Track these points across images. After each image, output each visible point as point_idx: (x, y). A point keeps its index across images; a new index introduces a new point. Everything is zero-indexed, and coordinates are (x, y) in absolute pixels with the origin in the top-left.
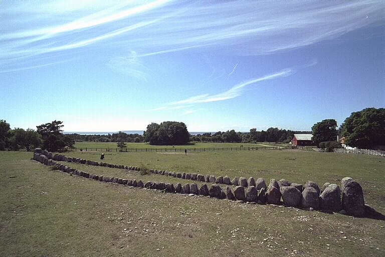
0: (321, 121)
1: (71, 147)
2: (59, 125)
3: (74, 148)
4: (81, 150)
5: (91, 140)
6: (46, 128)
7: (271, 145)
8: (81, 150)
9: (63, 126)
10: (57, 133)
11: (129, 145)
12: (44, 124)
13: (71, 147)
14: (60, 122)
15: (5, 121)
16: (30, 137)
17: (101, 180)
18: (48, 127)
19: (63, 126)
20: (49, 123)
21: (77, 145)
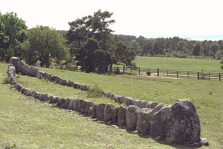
0: (62, 30)
1: (129, 63)
2: (107, 20)
3: (135, 68)
4: (149, 74)
5: (206, 54)
6: (84, 25)
7: (142, 73)
8: (149, 74)
9: (113, 21)
10: (106, 35)
11: (140, 61)
12: (81, 18)
13: (129, 63)
14: (107, 15)
15: (7, 13)
16: (47, 41)
17: (36, 96)
18: (88, 24)
19: (113, 21)
20: (90, 17)
21: (140, 61)
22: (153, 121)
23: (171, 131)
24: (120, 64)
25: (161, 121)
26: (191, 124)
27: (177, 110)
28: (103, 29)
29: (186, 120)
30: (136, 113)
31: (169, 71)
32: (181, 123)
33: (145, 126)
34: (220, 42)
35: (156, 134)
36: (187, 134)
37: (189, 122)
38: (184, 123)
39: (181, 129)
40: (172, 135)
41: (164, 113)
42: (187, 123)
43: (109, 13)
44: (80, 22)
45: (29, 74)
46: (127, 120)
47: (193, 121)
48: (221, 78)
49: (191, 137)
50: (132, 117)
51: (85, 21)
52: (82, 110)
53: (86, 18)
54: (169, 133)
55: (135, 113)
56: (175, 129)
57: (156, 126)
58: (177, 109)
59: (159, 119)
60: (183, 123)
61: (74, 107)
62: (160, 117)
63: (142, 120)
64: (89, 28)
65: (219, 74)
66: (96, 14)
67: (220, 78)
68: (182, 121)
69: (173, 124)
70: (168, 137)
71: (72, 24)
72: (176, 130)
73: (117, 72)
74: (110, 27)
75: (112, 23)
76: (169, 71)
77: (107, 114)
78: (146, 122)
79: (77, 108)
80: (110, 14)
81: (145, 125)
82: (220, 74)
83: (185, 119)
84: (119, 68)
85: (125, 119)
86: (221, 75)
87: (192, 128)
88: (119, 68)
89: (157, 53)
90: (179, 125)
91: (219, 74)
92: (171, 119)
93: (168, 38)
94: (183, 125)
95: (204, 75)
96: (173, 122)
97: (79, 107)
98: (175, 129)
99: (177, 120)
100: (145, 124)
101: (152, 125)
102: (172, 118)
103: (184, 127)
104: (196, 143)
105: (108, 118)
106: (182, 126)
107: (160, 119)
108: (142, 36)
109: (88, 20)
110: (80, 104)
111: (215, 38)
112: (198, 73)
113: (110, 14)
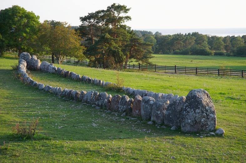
2: (122, 14)
26: (206, 113)
27: (193, 100)
30: (151, 104)
31: (187, 68)
32: (196, 113)
34: (243, 37)
36: (202, 124)
37: (205, 112)
38: (200, 112)
39: (196, 119)
42: (203, 112)
45: (41, 69)
47: (209, 111)
48: (243, 75)
49: (207, 126)
52: (96, 103)
56: (190, 119)
58: (193, 99)
59: (174, 109)
60: (198, 113)
61: (88, 100)
63: (157, 110)
65: (241, 71)
67: (242, 75)
68: (197, 111)
69: (188, 113)
70: (183, 127)
71: (83, 19)
74: (126, 23)
75: (128, 19)
76: (187, 68)
78: (161, 113)
79: (91, 101)
80: (127, 8)
82: (242, 71)
85: (140, 110)
86: (243, 71)
87: (207, 117)
90: (194, 114)
91: (241, 71)
92: (186, 108)
93: (187, 34)
94: (198, 115)
95: (224, 70)
99: (192, 110)
102: (187, 108)
103: (199, 116)
104: (212, 133)
106: (197, 115)
107: (175, 109)
108: (159, 32)
109: (102, 14)
111: (239, 34)
112: (219, 69)
113: (127, 8)
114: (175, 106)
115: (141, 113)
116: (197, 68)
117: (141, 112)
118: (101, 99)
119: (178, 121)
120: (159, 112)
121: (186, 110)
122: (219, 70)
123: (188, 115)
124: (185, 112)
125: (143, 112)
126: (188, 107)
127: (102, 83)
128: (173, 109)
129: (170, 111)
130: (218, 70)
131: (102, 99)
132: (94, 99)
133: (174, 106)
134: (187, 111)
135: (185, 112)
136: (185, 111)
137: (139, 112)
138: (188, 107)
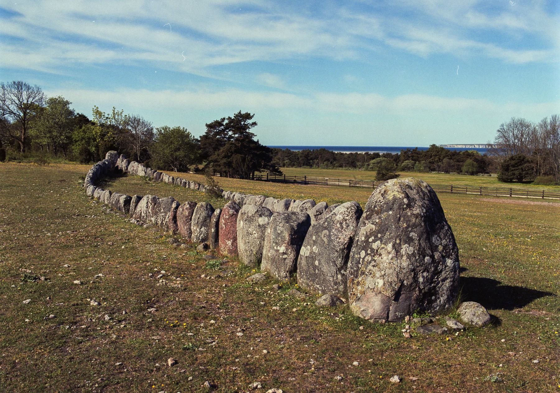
2: (250, 121)
12: (219, 119)
14: (248, 116)
18: (228, 127)
20: (229, 118)
22: (309, 247)
23: (369, 282)
24: (263, 171)
25: (334, 245)
27: (391, 213)
28: (244, 133)
29: (420, 244)
33: (285, 259)
35: (318, 286)
40: (370, 294)
41: (341, 224)
43: (249, 114)
44: (218, 124)
46: (238, 241)
50: (249, 234)
51: (224, 123)
53: (224, 119)
54: (359, 288)
55: (259, 225)
56: (383, 276)
57: (317, 263)
61: (143, 214)
62: (330, 236)
63: (276, 243)
64: (228, 130)
66: (236, 116)
71: (209, 126)
72: (386, 278)
73: (260, 179)
74: (251, 130)
77: (198, 226)
81: (285, 256)
83: (416, 242)
84: (262, 176)
85: (235, 239)
88: (262, 176)
89: (304, 165)
92: (367, 241)
96: (375, 253)
97: (150, 213)
98: (383, 276)
100: (284, 253)
101: (303, 258)
102: (370, 240)
105: (200, 238)
107: (330, 241)
110: (151, 207)
114: (330, 232)
115: (237, 247)
116: (481, 188)
117: (237, 243)
118: (160, 211)
119: (339, 276)
120: (155, 306)
121: (366, 246)
122: (450, 191)
123: (373, 263)
124: (363, 252)
125: (241, 246)
126: (376, 236)
127: (399, 175)
128: (325, 240)
129: (314, 248)
130: (453, 191)
131: (162, 211)
132: (151, 212)
133: (326, 232)
134: (372, 250)
135: (363, 252)
136: (365, 248)
137: (232, 244)
138: (376, 236)
